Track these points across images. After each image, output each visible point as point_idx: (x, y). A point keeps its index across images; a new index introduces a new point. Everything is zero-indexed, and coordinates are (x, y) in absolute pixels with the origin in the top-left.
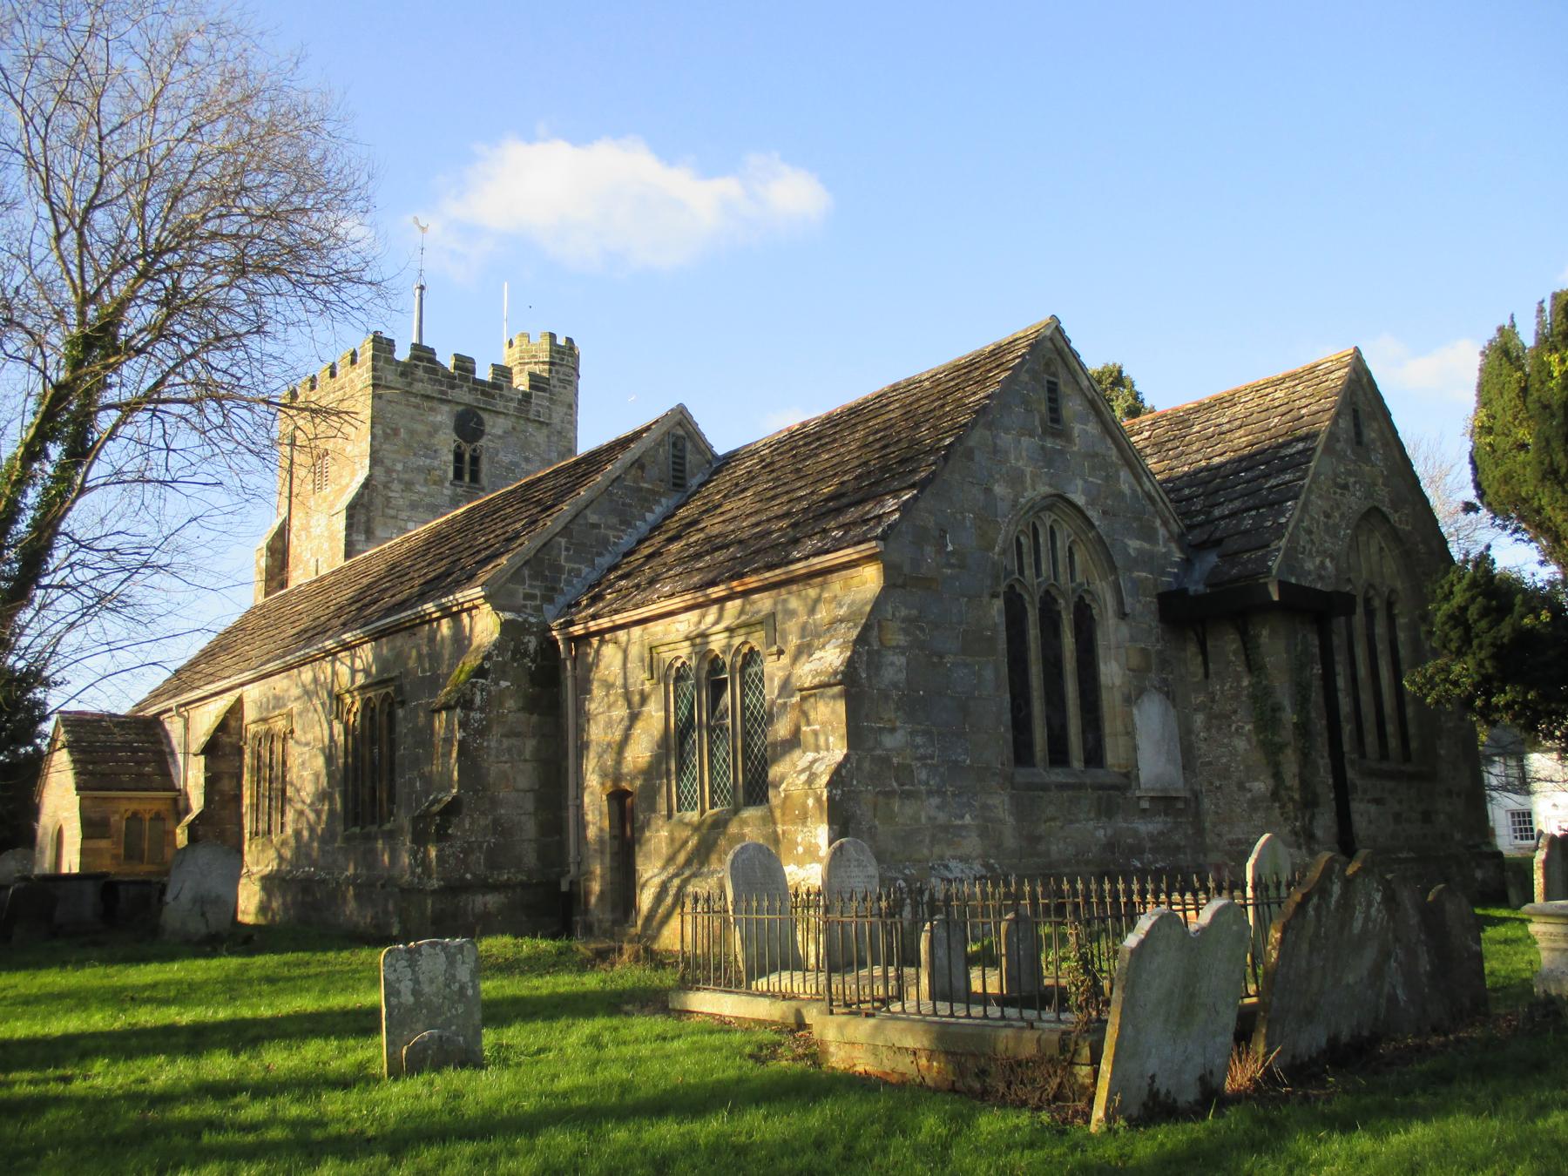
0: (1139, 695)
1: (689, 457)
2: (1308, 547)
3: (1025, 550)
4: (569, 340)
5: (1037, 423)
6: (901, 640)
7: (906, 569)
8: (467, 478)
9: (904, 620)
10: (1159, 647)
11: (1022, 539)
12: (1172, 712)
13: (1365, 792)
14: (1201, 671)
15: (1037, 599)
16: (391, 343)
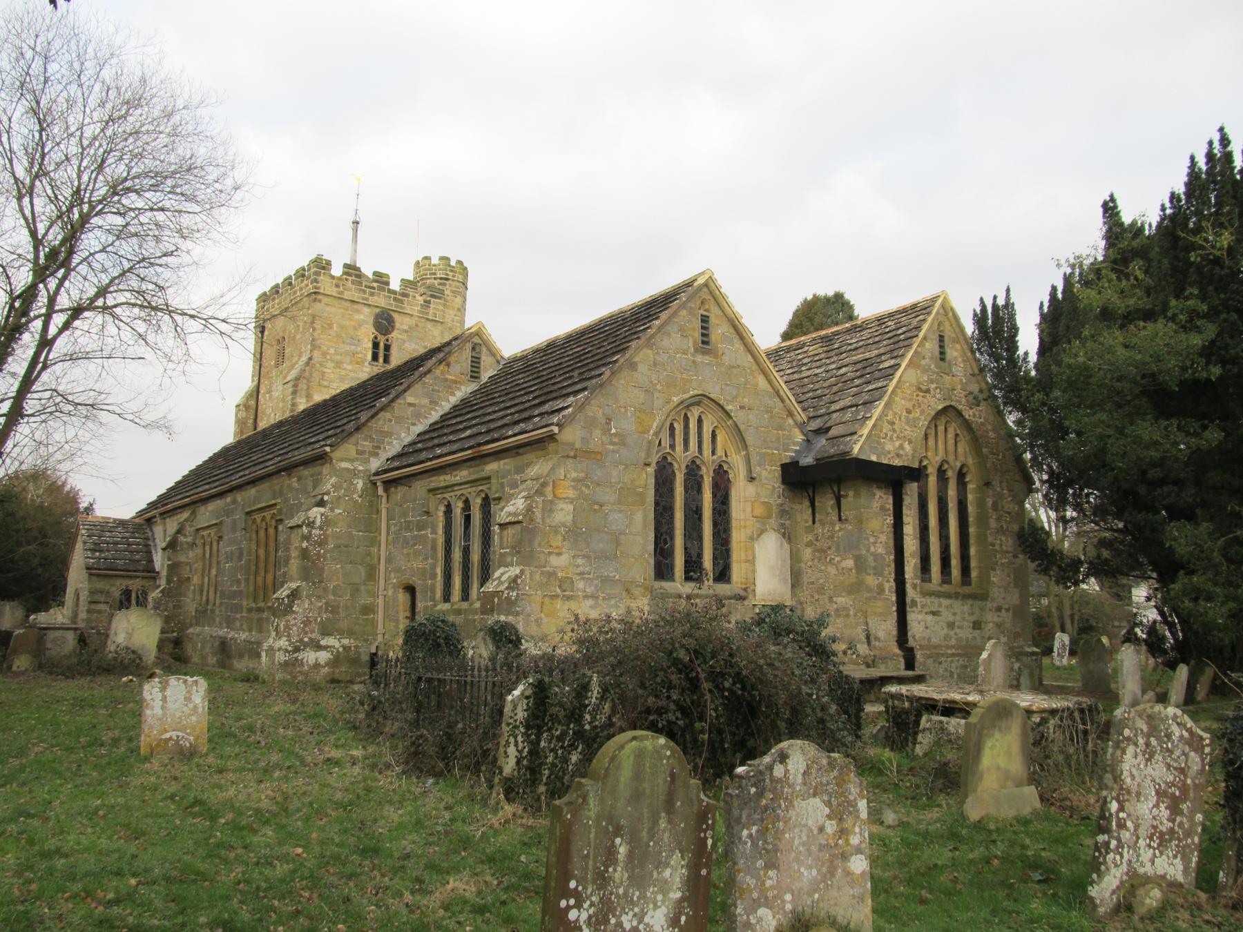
0: (759, 535)
1: (483, 358)
2: (890, 434)
3: (677, 432)
4: (460, 262)
5: (691, 344)
6: (571, 493)
7: (577, 445)
8: (381, 360)
9: (574, 480)
10: (780, 501)
11: (676, 425)
12: (787, 546)
13: (923, 606)
14: (811, 520)
15: (683, 467)
16: (329, 263)
